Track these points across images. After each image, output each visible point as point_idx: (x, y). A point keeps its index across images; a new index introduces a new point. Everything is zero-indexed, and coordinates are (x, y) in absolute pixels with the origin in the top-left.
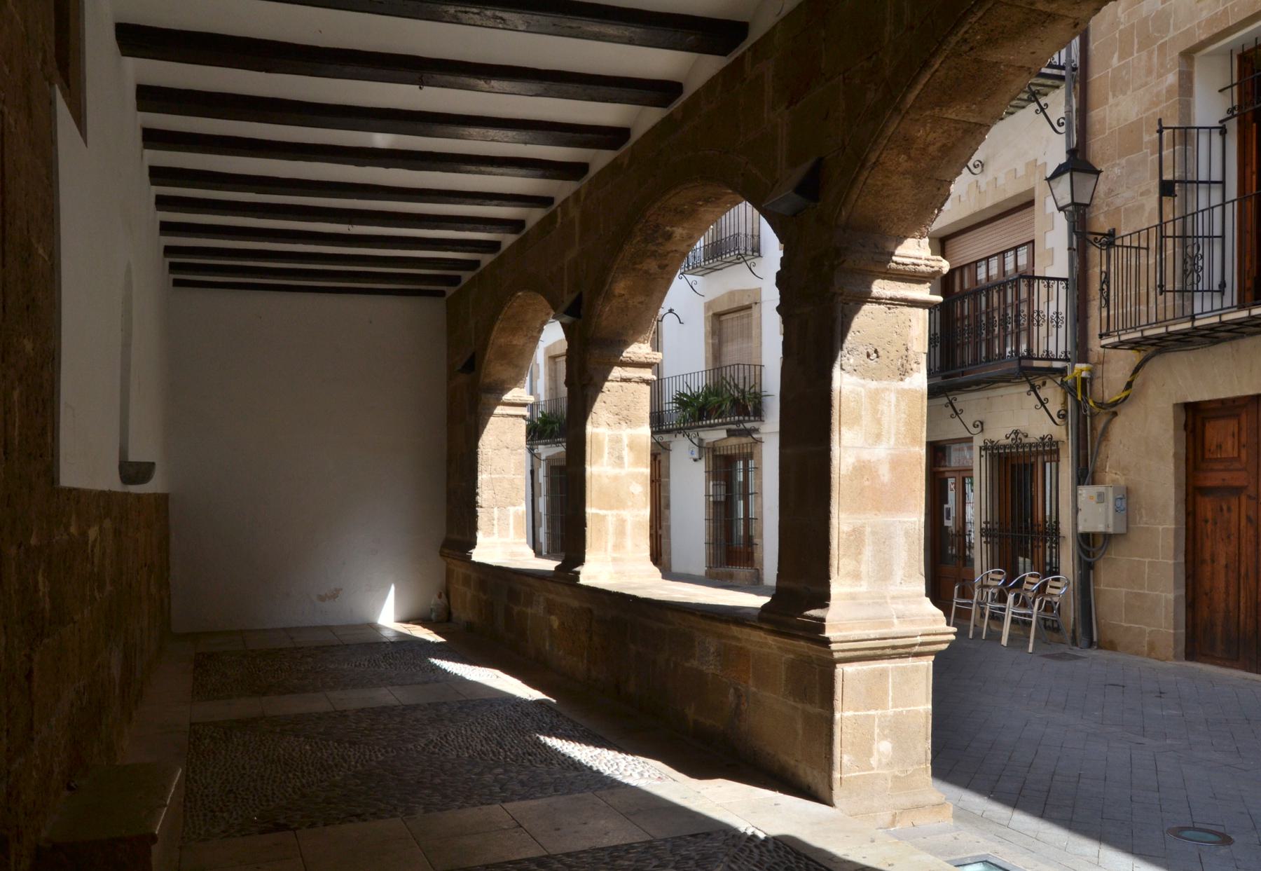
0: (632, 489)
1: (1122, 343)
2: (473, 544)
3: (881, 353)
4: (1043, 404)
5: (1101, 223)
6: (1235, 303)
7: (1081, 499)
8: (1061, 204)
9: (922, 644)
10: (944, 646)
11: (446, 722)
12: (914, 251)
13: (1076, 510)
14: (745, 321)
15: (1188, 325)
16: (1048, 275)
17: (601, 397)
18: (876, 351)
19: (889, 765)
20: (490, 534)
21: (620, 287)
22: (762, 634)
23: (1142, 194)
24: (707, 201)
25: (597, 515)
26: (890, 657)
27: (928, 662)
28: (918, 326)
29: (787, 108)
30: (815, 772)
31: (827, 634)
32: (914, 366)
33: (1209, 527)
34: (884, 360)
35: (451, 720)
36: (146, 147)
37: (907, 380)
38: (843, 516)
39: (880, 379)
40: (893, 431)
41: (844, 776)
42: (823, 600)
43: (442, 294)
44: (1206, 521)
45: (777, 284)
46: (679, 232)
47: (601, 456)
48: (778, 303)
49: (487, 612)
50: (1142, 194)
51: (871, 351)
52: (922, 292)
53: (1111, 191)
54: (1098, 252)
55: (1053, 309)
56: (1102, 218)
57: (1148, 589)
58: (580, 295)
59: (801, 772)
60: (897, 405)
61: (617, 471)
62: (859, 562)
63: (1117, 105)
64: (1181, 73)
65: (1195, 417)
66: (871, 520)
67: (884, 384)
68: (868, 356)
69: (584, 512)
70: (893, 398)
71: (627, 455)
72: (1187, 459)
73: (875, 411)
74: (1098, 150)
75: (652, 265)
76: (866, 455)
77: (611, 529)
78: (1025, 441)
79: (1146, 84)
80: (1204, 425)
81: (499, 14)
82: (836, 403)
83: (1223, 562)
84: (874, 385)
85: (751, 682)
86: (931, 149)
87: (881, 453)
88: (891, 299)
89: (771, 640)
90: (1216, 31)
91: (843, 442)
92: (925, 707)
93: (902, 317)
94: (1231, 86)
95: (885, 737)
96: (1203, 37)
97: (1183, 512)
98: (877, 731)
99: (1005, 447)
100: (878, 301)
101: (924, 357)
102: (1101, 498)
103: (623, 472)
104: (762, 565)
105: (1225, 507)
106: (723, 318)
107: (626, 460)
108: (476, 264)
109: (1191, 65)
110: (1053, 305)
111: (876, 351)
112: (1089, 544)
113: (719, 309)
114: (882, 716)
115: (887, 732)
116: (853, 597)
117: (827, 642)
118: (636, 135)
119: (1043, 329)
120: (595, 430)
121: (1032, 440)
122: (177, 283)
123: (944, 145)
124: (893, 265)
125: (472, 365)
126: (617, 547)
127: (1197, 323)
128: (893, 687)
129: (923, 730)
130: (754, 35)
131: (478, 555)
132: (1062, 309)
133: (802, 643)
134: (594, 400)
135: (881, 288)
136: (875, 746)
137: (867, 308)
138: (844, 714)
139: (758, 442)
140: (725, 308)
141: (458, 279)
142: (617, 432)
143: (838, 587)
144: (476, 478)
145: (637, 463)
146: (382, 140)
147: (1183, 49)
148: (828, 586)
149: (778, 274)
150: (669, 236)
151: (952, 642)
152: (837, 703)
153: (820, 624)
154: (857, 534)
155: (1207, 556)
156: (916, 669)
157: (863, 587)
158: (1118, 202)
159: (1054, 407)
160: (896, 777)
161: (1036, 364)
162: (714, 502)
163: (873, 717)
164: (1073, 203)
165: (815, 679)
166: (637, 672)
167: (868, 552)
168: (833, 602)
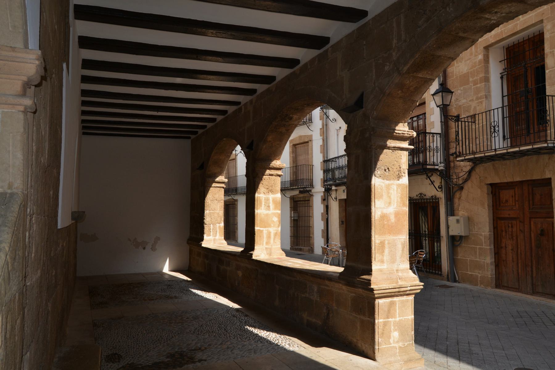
0: (273, 219)
1: (465, 160)
2: (202, 239)
3: (390, 169)
4: (432, 183)
5: (453, 111)
6: (509, 145)
7: (449, 222)
8: (438, 105)
9: (410, 290)
10: (419, 291)
11: (200, 319)
12: (402, 128)
13: (448, 227)
14: (306, 147)
15: (494, 153)
16: (432, 132)
17: (262, 182)
18: (388, 169)
19: (398, 342)
20: (209, 235)
21: (270, 138)
22: (341, 285)
23: (470, 101)
24: (308, 105)
25: (259, 230)
26: (397, 296)
27: (412, 298)
28: (404, 159)
29: (348, 71)
30: (366, 346)
31: (372, 287)
32: (403, 174)
33: (504, 233)
34: (391, 172)
35: (202, 318)
36: (82, 83)
37: (401, 180)
38: (376, 236)
39: (390, 180)
40: (396, 201)
41: (380, 347)
42: (369, 272)
43: (189, 138)
44: (502, 231)
45: (344, 140)
46: (295, 117)
47: (261, 206)
48: (345, 148)
49: (211, 270)
50: (470, 101)
51: (386, 168)
52: (405, 145)
53: (457, 99)
54: (454, 123)
55: (435, 145)
56: (454, 110)
57: (480, 259)
58: (253, 141)
59: (360, 345)
60: (397, 190)
61: (268, 212)
62: (383, 256)
63: (458, 67)
64: (484, 55)
65: (495, 190)
66: (388, 238)
67: (392, 182)
68: (385, 170)
69: (254, 229)
70: (395, 187)
71: (272, 206)
72: (493, 206)
73: (388, 193)
74: (450, 85)
75: (283, 130)
76: (385, 211)
77: (265, 236)
78: (425, 197)
79: (470, 59)
80: (499, 193)
81: (233, 33)
82: (373, 190)
83: (510, 248)
84: (387, 182)
85: (334, 304)
86: (411, 88)
87: (391, 210)
88: (394, 147)
89: (344, 287)
90: (498, 39)
91: (376, 206)
92: (411, 317)
93: (398, 154)
94: (504, 60)
95: (395, 330)
96: (493, 42)
97: (492, 226)
98: (392, 327)
99: (416, 200)
100: (389, 148)
101: (407, 170)
102: (458, 221)
103: (270, 212)
104: (313, 245)
105: (510, 225)
106: (297, 146)
107: (271, 207)
108: (205, 127)
109: (488, 52)
110: (435, 143)
111: (388, 169)
112: (454, 241)
113: (295, 143)
114: (395, 321)
115: (396, 328)
116: (381, 270)
117: (372, 290)
118: (278, 79)
119: (432, 153)
120: (259, 195)
121: (428, 197)
122: (84, 133)
123: (416, 87)
124: (395, 134)
125: (202, 167)
126: (267, 243)
127: (497, 153)
128: (399, 309)
129: (411, 327)
130: (332, 43)
131: (204, 244)
132: (439, 145)
133: (360, 290)
134: (259, 184)
135: (391, 143)
136: (392, 334)
137: (385, 151)
138: (379, 321)
139: (312, 195)
140: (298, 142)
141: (197, 132)
142: (268, 196)
143: (375, 266)
144: (204, 212)
145: (275, 208)
146: (179, 80)
147: (485, 46)
148: (371, 266)
149: (345, 136)
150: (291, 119)
151: (422, 289)
152: (376, 316)
153: (369, 282)
154: (382, 243)
155: (503, 245)
156: (407, 301)
157: (385, 266)
158: (460, 104)
159: (437, 184)
160: (400, 347)
161: (428, 167)
162: (294, 220)
163: (391, 321)
164: (443, 104)
165: (365, 303)
166: (277, 297)
167: (387, 251)
168: (373, 273)
